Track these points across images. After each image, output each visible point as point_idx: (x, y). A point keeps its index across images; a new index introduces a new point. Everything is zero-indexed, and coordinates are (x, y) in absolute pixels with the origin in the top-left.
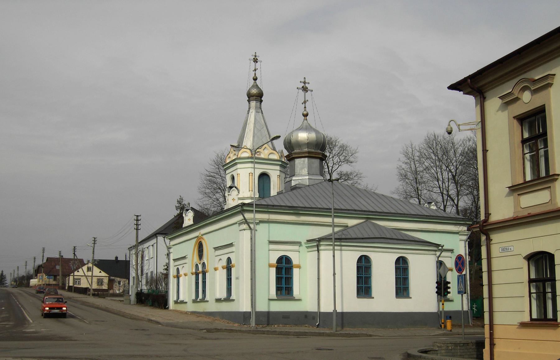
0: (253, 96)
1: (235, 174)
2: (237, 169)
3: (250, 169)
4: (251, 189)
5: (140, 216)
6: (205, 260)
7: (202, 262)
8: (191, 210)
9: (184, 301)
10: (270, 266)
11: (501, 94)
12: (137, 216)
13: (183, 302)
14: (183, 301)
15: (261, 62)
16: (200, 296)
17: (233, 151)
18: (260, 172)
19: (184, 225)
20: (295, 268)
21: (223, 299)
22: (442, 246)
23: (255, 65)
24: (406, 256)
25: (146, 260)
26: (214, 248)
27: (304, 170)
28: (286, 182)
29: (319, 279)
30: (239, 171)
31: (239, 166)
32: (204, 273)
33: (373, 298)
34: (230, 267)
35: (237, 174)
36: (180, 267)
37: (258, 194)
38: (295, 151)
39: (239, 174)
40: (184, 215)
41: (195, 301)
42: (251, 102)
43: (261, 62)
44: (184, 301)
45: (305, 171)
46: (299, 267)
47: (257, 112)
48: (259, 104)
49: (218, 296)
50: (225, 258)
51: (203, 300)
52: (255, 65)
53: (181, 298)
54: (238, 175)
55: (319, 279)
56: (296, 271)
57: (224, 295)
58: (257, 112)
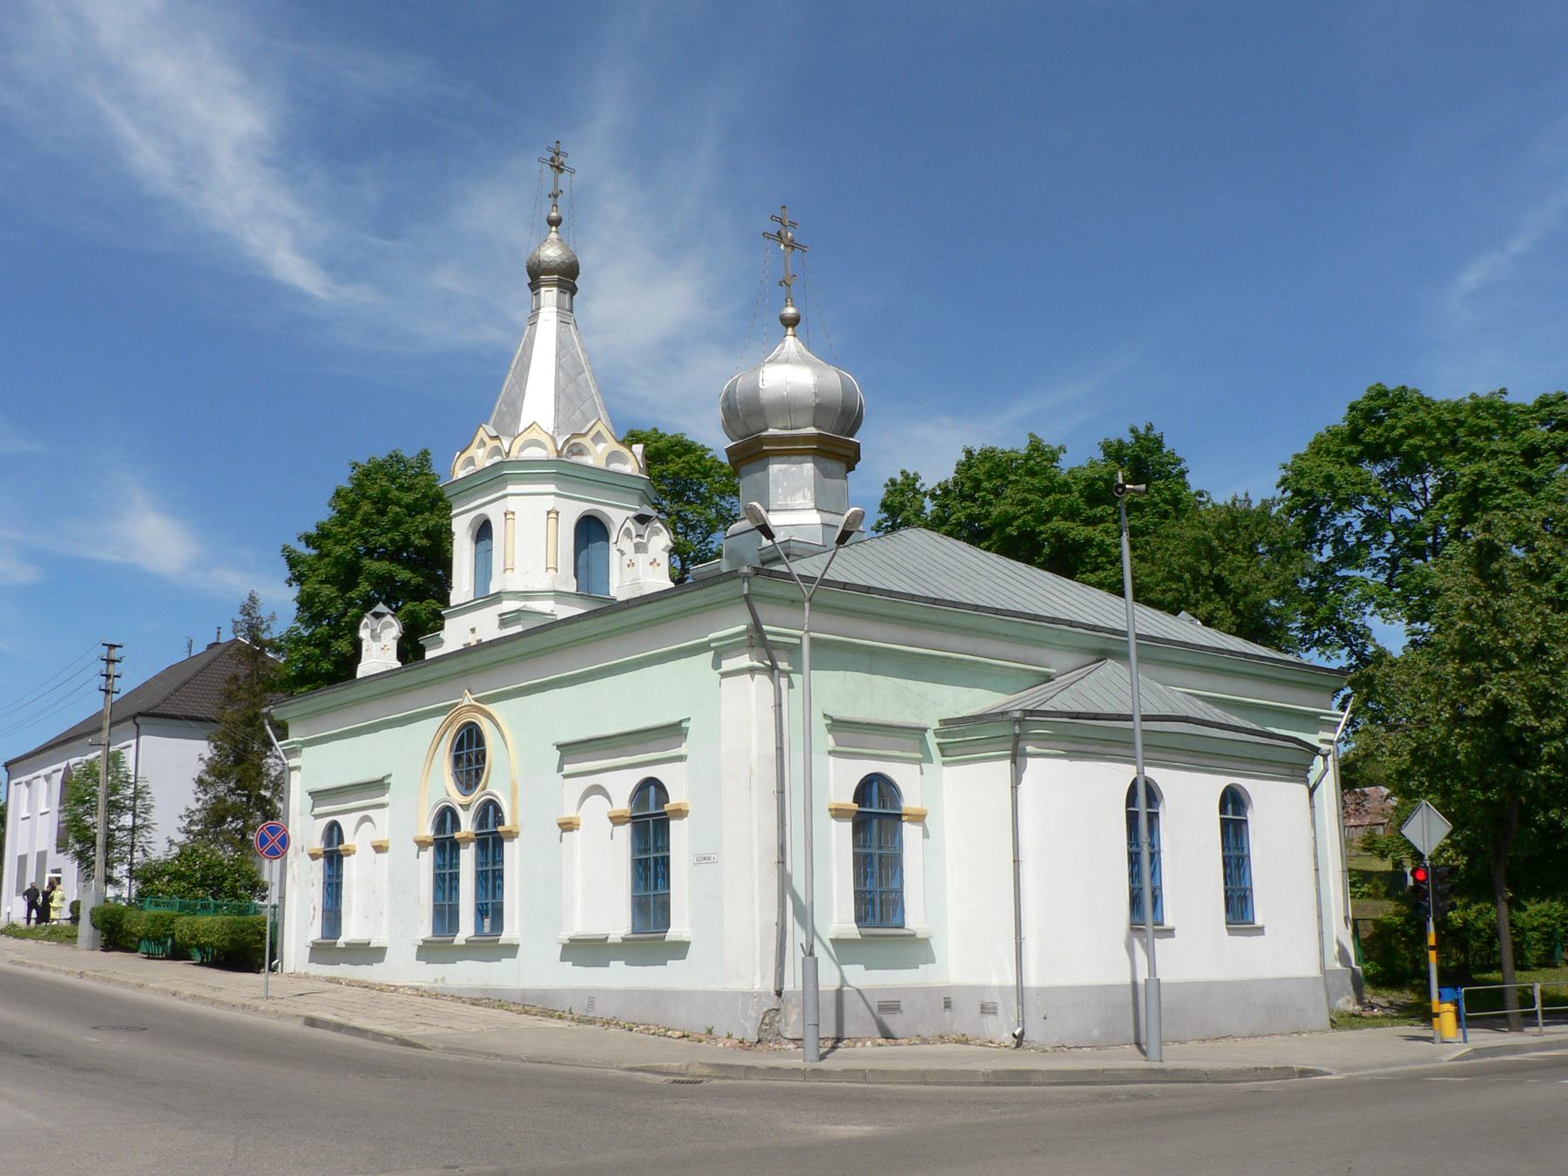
0: (549, 271)
1: (494, 513)
2: (505, 496)
3: (553, 497)
4: (551, 565)
5: (121, 647)
6: (496, 784)
7: (477, 797)
8: (393, 615)
9: (371, 945)
10: (422, 844)
11: (466, 505)
12: (112, 646)
13: (367, 953)
14: (369, 943)
15: (572, 172)
16: (467, 927)
17: (487, 439)
18: (583, 511)
19: (363, 670)
20: (908, 821)
21: (344, 946)
22: (1324, 753)
23: (556, 180)
24: (1243, 785)
25: (42, 814)
26: (559, 747)
27: (801, 494)
28: (730, 537)
29: (1016, 861)
30: (511, 504)
31: (510, 489)
32: (491, 843)
33: (1260, 931)
34: (665, 813)
35: (506, 514)
36: (347, 823)
37: (575, 581)
38: (770, 430)
39: (513, 513)
40: (364, 633)
41: (427, 952)
42: (543, 290)
43: (572, 172)
44: (371, 945)
45: (805, 498)
46: (919, 818)
47: (562, 322)
48: (567, 296)
49: (580, 927)
50: (622, 785)
51: (490, 945)
52: (556, 180)
53: (352, 930)
54: (509, 516)
55: (1016, 861)
56: (910, 831)
57: (617, 922)
58: (562, 322)
